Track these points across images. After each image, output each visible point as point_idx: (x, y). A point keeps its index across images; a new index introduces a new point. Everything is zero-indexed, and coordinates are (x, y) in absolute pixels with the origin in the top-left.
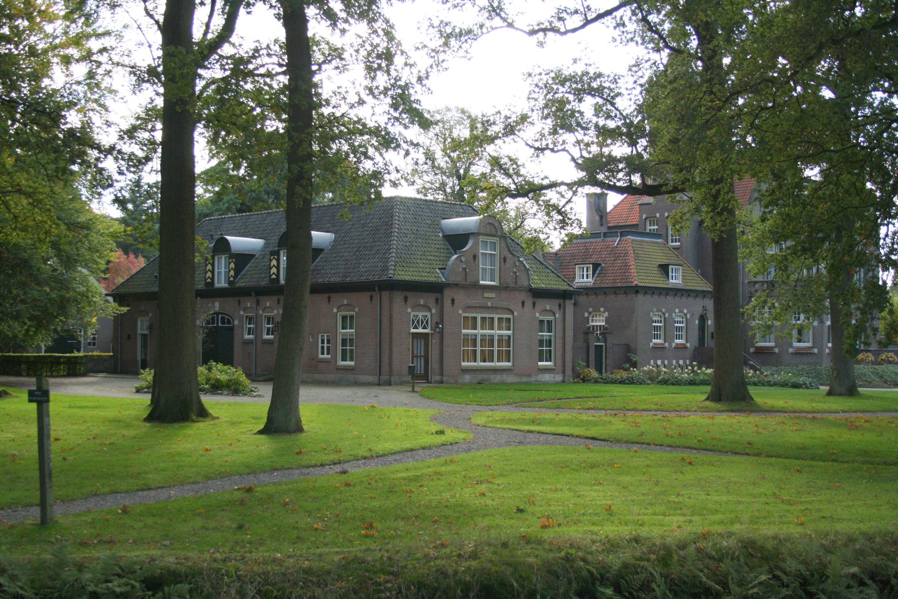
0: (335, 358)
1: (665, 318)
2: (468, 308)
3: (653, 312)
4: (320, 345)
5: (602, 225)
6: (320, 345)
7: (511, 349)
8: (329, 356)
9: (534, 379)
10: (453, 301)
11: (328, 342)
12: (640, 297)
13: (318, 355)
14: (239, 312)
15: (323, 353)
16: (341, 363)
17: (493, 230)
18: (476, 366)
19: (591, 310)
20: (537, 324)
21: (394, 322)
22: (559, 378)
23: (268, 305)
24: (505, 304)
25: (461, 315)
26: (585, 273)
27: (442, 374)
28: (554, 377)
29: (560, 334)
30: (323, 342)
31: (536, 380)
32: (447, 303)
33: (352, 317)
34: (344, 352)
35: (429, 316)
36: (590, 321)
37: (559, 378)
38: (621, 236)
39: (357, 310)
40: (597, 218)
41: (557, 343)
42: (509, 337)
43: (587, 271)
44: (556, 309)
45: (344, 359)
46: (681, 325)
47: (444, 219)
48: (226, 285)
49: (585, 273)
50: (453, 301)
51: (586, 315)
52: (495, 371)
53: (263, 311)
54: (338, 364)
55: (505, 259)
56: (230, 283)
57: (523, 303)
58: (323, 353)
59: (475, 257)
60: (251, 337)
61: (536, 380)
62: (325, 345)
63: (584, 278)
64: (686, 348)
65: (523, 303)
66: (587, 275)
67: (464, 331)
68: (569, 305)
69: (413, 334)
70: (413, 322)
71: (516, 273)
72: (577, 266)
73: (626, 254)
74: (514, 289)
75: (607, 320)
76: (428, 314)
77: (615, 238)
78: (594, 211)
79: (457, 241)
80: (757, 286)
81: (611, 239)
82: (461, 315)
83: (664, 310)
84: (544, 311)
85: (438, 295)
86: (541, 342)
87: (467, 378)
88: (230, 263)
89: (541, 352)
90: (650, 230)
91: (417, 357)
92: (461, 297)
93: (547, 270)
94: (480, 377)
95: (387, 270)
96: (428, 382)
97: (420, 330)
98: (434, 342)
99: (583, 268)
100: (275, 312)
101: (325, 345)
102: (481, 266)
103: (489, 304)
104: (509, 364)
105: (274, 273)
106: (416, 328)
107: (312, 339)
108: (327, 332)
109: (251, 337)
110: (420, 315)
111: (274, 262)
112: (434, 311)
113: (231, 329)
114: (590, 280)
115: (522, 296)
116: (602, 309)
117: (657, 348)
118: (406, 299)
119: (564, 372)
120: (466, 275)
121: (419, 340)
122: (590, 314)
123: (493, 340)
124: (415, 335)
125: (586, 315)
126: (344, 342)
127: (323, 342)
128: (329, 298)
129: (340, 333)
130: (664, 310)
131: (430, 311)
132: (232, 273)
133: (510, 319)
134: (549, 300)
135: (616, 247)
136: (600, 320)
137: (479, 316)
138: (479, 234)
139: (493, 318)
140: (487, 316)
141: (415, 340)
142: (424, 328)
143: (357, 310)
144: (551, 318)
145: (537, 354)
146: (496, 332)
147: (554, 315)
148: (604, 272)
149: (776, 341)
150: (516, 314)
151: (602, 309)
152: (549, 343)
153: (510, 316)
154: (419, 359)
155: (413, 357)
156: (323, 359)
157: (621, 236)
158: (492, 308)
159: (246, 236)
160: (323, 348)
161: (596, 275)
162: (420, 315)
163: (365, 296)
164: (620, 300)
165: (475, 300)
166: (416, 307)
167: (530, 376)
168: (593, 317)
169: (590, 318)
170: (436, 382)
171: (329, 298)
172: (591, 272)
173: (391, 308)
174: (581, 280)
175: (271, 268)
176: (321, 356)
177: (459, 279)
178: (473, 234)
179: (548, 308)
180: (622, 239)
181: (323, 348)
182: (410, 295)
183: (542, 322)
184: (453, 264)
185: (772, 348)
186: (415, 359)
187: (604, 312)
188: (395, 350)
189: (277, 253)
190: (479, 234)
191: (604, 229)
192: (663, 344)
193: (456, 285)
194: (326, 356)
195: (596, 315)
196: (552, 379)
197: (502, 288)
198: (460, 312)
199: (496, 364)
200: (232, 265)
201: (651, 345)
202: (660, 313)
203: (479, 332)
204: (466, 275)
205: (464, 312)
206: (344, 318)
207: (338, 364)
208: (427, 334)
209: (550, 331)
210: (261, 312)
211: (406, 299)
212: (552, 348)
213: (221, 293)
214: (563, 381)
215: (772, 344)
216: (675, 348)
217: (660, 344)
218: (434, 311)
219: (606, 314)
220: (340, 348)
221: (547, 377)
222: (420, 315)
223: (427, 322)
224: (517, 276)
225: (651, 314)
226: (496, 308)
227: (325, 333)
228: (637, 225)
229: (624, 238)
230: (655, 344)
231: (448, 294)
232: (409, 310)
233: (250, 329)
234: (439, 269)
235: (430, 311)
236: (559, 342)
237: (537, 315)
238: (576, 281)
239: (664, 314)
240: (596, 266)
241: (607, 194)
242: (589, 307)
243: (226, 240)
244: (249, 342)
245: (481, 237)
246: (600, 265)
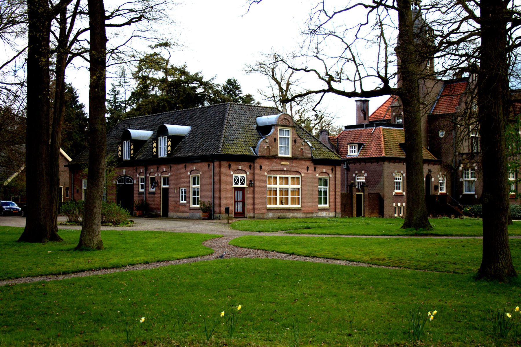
0: (189, 203)
1: (403, 177)
2: (270, 172)
3: (395, 173)
4: (181, 195)
5: (365, 119)
6: (181, 195)
7: (300, 196)
8: (186, 202)
9: (315, 215)
10: (261, 167)
11: (185, 193)
12: (386, 164)
13: (179, 201)
14: (137, 175)
15: (182, 200)
16: (193, 206)
17: (287, 123)
18: (276, 208)
19: (357, 172)
20: (317, 182)
21: (222, 180)
22: (332, 214)
23: (152, 171)
24: (296, 169)
25: (266, 176)
26: (353, 149)
27: (254, 213)
28: (329, 214)
29: (333, 188)
30: (182, 193)
31: (317, 216)
32: (257, 168)
33: (198, 177)
34: (194, 199)
35: (245, 176)
36: (356, 179)
37: (332, 214)
38: (376, 127)
39: (201, 173)
40: (362, 115)
41: (331, 193)
42: (299, 189)
43: (355, 148)
44: (329, 171)
45: (194, 204)
46: (399, 181)
47: (259, 116)
48: (129, 159)
49: (353, 149)
50: (261, 167)
51: (354, 175)
52: (289, 210)
53: (149, 174)
54: (191, 206)
55: (295, 141)
56: (131, 157)
57: (308, 168)
58: (182, 200)
59: (275, 140)
60: (143, 190)
61: (317, 216)
62: (184, 195)
63: (353, 153)
64: (403, 195)
65: (308, 168)
66: (355, 150)
67: (268, 186)
68: (338, 170)
69: (234, 187)
70: (235, 180)
71: (302, 149)
72: (348, 145)
73: (379, 137)
74: (301, 159)
75: (366, 179)
76: (245, 176)
77: (372, 128)
78: (360, 111)
79: (264, 130)
80: (464, 156)
81: (370, 128)
82: (266, 176)
83: (402, 172)
84: (322, 173)
85: (252, 164)
86: (320, 192)
87: (271, 215)
88: (168, 142)
89: (320, 198)
90: (398, 122)
91: (238, 201)
92: (266, 164)
93: (325, 148)
94: (279, 214)
95: (218, 148)
96: (245, 217)
97: (239, 185)
98: (248, 193)
99: (352, 146)
100: (156, 175)
101: (184, 195)
102: (279, 146)
103: (285, 169)
104: (300, 206)
105: (155, 152)
106: (236, 184)
107: (177, 191)
108: (184, 187)
109: (143, 190)
110: (239, 176)
111: (155, 145)
112: (248, 173)
113: (133, 185)
114: (356, 153)
115: (308, 164)
116: (363, 172)
117: (397, 195)
118: (230, 166)
119: (335, 211)
120: (269, 151)
121: (239, 192)
122: (356, 174)
123: (288, 191)
124: (236, 189)
125: (354, 175)
126: (194, 193)
127: (182, 193)
128: (185, 166)
129: (192, 187)
130: (402, 172)
131: (246, 173)
132: (169, 148)
133: (299, 178)
134: (324, 166)
135: (373, 133)
136: (362, 179)
137: (290, 177)
138: (278, 125)
139: (276, 177)
140: (284, 176)
141: (236, 192)
142: (242, 184)
143: (201, 173)
144: (326, 177)
145: (317, 200)
146: (290, 186)
147: (329, 175)
148: (365, 148)
149: (475, 191)
150: (303, 175)
151: (363, 172)
152: (325, 193)
153: (300, 176)
154: (239, 203)
155: (235, 202)
156: (182, 203)
157: (376, 127)
158: (287, 171)
159: (144, 129)
160: (182, 196)
161: (360, 151)
162: (239, 176)
163: (205, 165)
164: (374, 166)
165: (275, 165)
166: (237, 171)
167: (312, 213)
168: (358, 177)
169: (357, 178)
170: (250, 217)
171: (185, 166)
172: (357, 149)
173: (220, 172)
174: (351, 154)
175: (153, 148)
176: (181, 202)
177: (264, 153)
178: (274, 125)
179: (324, 171)
180: (377, 128)
181: (182, 196)
182: (233, 164)
183: (321, 179)
184: (260, 144)
185: (473, 195)
186: (236, 204)
187: (364, 173)
188: (222, 198)
189: (122, 144)
190: (278, 125)
191: (366, 122)
192: (402, 193)
193: (263, 157)
194: (184, 202)
195: (360, 175)
196: (327, 215)
197: (294, 158)
198: (266, 174)
199: (290, 206)
200: (169, 143)
201: (394, 193)
202: (400, 174)
203: (278, 186)
204: (269, 151)
205: (268, 174)
206: (194, 178)
207: (191, 206)
208: (245, 187)
209: (326, 185)
210: (148, 175)
211: (230, 166)
212: (300, 196)
213: (163, 162)
214: (335, 216)
215: (473, 193)
216: (395, 195)
217: (400, 193)
218: (248, 173)
219: (366, 175)
220: (192, 196)
221: (324, 214)
222: (239, 176)
223: (244, 180)
224: (303, 152)
225: (394, 175)
226: (290, 171)
227: (183, 187)
228: (390, 120)
229: (378, 128)
230: (396, 193)
231: (258, 163)
232: (232, 173)
233: (142, 185)
234: (252, 147)
235: (246, 173)
236: (333, 192)
237: (317, 175)
238: (348, 154)
239: (402, 174)
240: (360, 145)
241: (368, 101)
242: (355, 171)
243: (166, 127)
244: (142, 193)
245: (279, 127)
246: (363, 144)
